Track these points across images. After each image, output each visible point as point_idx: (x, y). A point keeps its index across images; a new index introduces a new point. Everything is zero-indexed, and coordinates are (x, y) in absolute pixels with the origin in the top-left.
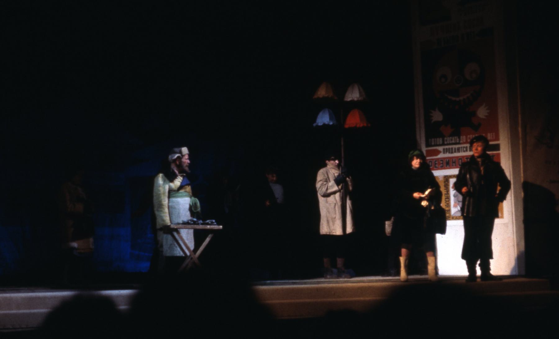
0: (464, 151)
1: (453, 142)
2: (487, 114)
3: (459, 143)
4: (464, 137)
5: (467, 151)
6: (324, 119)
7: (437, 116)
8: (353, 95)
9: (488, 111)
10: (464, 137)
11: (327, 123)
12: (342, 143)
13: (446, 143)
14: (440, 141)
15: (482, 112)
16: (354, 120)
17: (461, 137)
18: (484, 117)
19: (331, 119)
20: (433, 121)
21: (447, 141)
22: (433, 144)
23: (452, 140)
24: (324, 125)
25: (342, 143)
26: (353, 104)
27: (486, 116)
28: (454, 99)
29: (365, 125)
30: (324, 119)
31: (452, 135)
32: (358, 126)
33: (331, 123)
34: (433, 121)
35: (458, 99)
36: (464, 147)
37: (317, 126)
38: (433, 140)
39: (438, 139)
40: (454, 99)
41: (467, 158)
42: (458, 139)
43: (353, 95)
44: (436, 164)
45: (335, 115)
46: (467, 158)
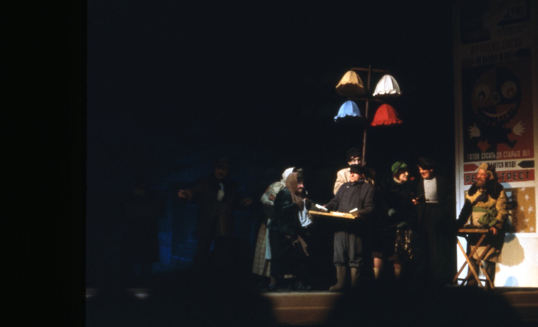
0: (500, 167)
1: (490, 157)
2: (523, 132)
3: (495, 159)
4: (501, 153)
5: (503, 166)
6: (346, 110)
7: (475, 132)
8: (386, 86)
9: (524, 129)
10: (501, 153)
11: (349, 114)
12: (364, 142)
13: (482, 158)
14: (477, 156)
15: (518, 130)
16: (383, 116)
17: (498, 153)
18: (520, 134)
19: (354, 110)
20: (471, 137)
21: (483, 156)
22: (471, 159)
23: (488, 155)
24: (347, 116)
25: (364, 142)
26: (386, 98)
27: (522, 134)
28: (491, 115)
29: (394, 122)
30: (346, 110)
31: (489, 151)
32: (386, 124)
33: (355, 115)
34: (471, 137)
35: (494, 116)
36: (500, 163)
37: (339, 118)
38: (471, 155)
39: (476, 154)
40: (491, 115)
41: (503, 174)
42: (494, 155)
43: (386, 86)
44: (473, 178)
45: (360, 105)
46: (503, 174)
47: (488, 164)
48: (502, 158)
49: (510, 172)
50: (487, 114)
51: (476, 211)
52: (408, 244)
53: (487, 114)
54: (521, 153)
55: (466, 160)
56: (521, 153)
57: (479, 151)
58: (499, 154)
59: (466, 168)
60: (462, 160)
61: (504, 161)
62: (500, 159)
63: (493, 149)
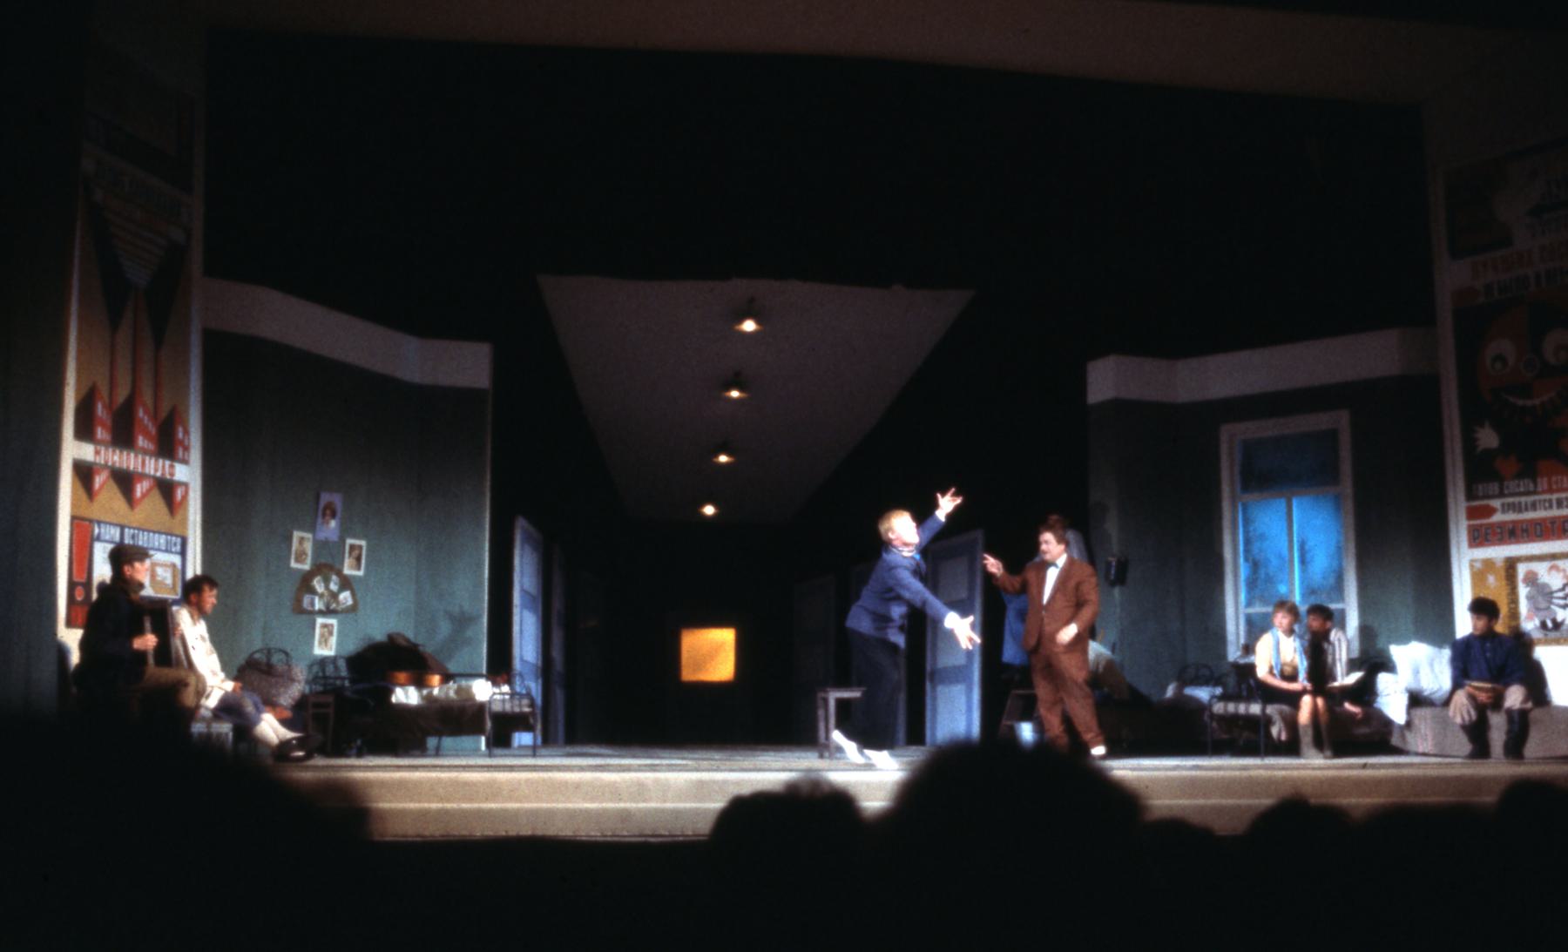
3: (1535, 493)
5: (1551, 507)
7: (1488, 438)
31: (1520, 476)
34: (1480, 449)
35: (1529, 403)
40: (1520, 402)
47: (1053, 564)
48: (1551, 491)
49: (1553, 520)
50: (1512, 399)
51: (172, 474)
52: (922, 514)
53: (1512, 399)
54: (1501, 489)
55: (1471, 495)
56: (1550, 484)
57: (1500, 479)
58: (1543, 483)
59: (1472, 513)
60: (1461, 496)
61: (1555, 496)
62: (1544, 492)
63: (1529, 471)
